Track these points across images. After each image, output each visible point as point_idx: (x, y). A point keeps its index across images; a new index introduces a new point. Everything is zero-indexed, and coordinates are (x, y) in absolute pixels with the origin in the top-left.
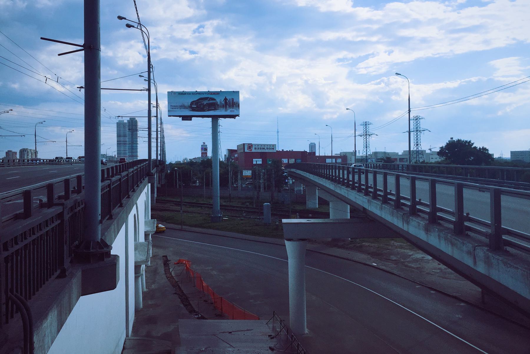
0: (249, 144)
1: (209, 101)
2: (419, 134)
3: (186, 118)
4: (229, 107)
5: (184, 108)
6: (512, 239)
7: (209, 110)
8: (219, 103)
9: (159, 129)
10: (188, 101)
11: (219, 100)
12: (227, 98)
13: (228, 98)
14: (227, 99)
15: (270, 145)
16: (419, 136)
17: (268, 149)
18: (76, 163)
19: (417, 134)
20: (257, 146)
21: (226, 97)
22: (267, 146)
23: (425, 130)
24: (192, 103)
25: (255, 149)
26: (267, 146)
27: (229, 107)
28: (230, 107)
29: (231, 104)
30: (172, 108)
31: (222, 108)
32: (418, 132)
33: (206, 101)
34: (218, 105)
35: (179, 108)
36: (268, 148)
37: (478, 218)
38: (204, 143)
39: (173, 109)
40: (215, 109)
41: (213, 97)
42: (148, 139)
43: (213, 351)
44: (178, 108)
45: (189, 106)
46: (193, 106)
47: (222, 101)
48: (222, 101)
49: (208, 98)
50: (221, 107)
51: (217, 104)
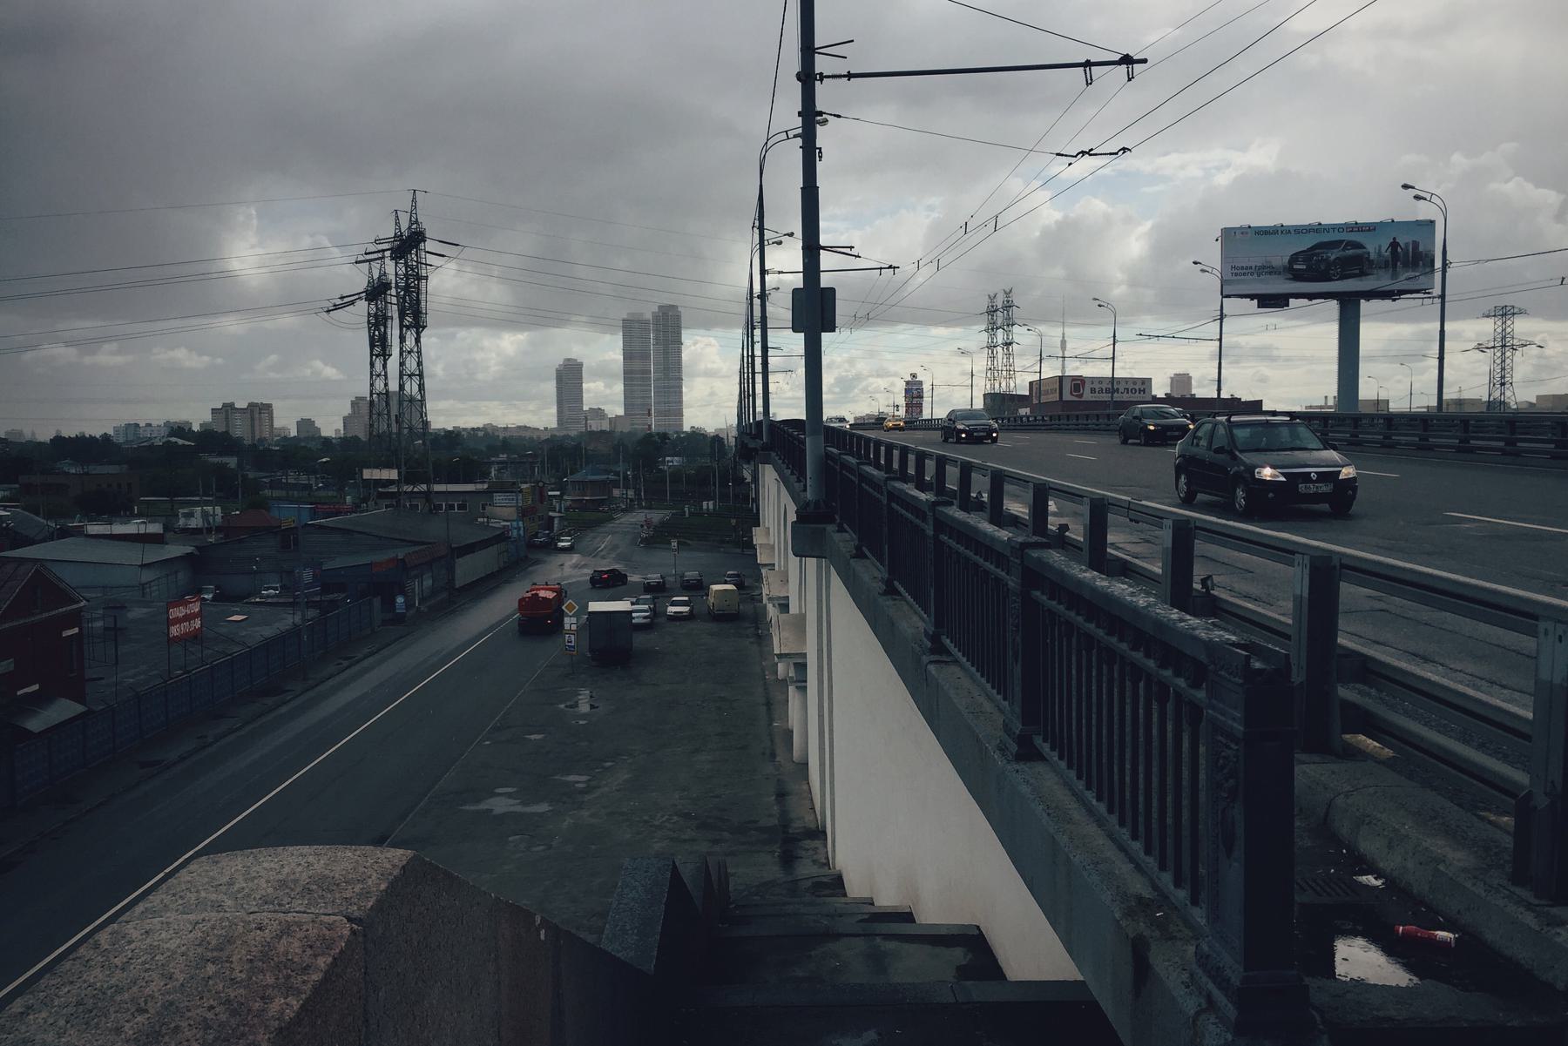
0: (1074, 378)
1: (1344, 249)
2: (1508, 354)
3: (1273, 302)
4: (1403, 267)
5: (1270, 273)
6: (1509, 701)
7: (1343, 277)
8: (1373, 256)
9: (757, 332)
10: (1281, 254)
11: (1375, 246)
12: (1397, 241)
13: (1401, 241)
14: (1398, 244)
15: (1134, 381)
16: (1508, 361)
17: (1128, 393)
18: (896, 428)
19: (1503, 354)
20: (1139, 383)
21: (1394, 239)
22: (1127, 382)
23: (1526, 345)
24: (1294, 258)
25: (1093, 391)
26: (1127, 382)
27: (1403, 267)
28: (1406, 265)
29: (1411, 259)
30: (1236, 275)
31: (1381, 272)
32: (1507, 348)
33: (1335, 251)
34: (1371, 262)
35: (1255, 275)
36: (1128, 389)
37: (1522, 621)
38: (914, 376)
39: (1239, 277)
40: (1362, 274)
41: (1358, 240)
42: (804, 360)
43: (170, 978)
44: (1252, 274)
45: (1285, 268)
46: (1295, 267)
47: (1383, 250)
48: (1383, 250)
49: (1341, 242)
50: (1380, 268)
51: (1368, 259)
